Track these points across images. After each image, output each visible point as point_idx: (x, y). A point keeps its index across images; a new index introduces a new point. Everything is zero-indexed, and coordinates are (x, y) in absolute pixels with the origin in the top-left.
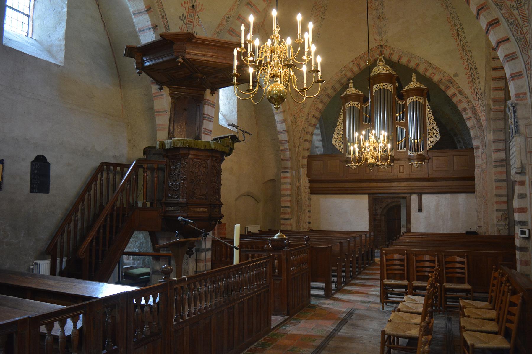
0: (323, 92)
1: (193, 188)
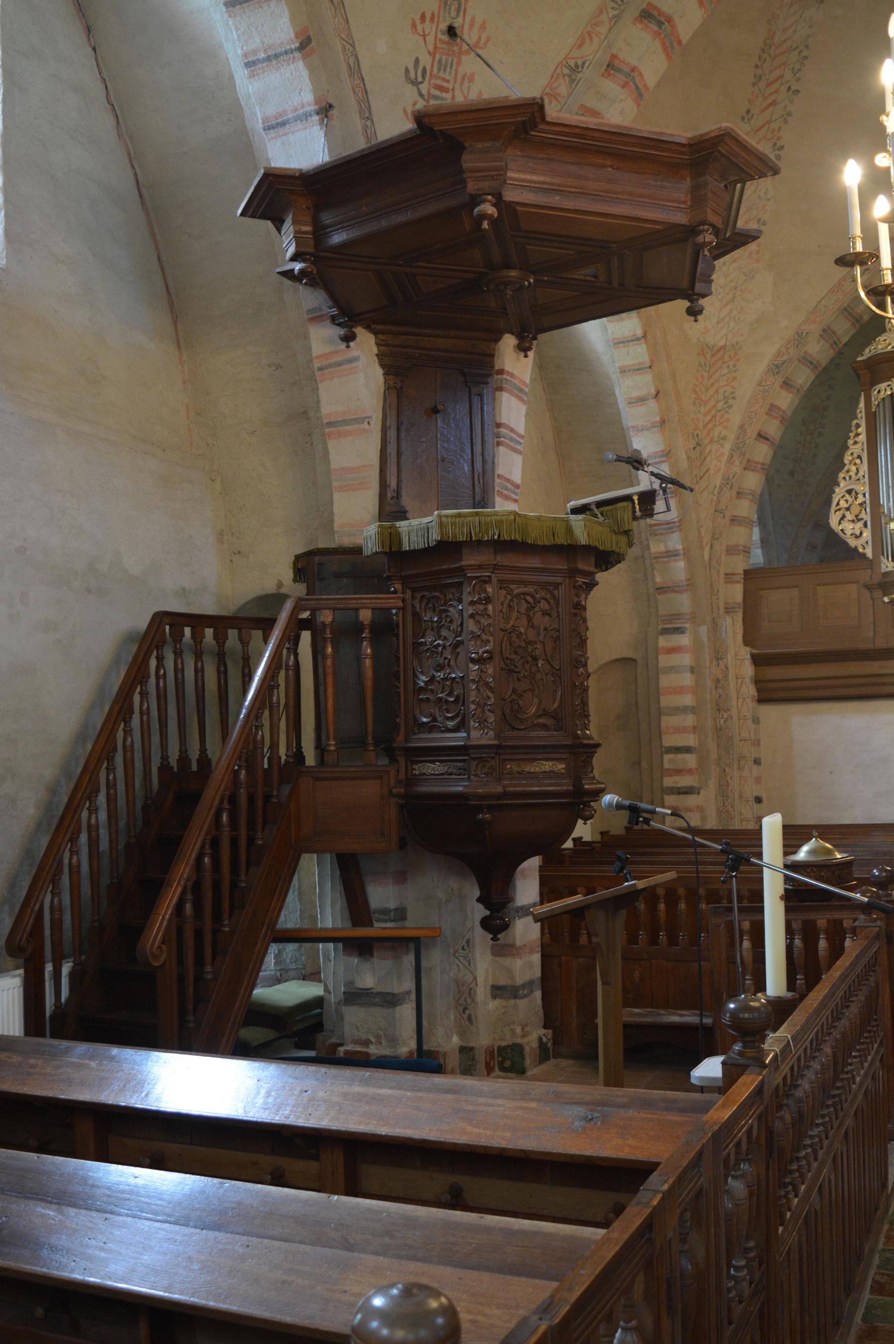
0: (791, 351)
1: (514, 691)
